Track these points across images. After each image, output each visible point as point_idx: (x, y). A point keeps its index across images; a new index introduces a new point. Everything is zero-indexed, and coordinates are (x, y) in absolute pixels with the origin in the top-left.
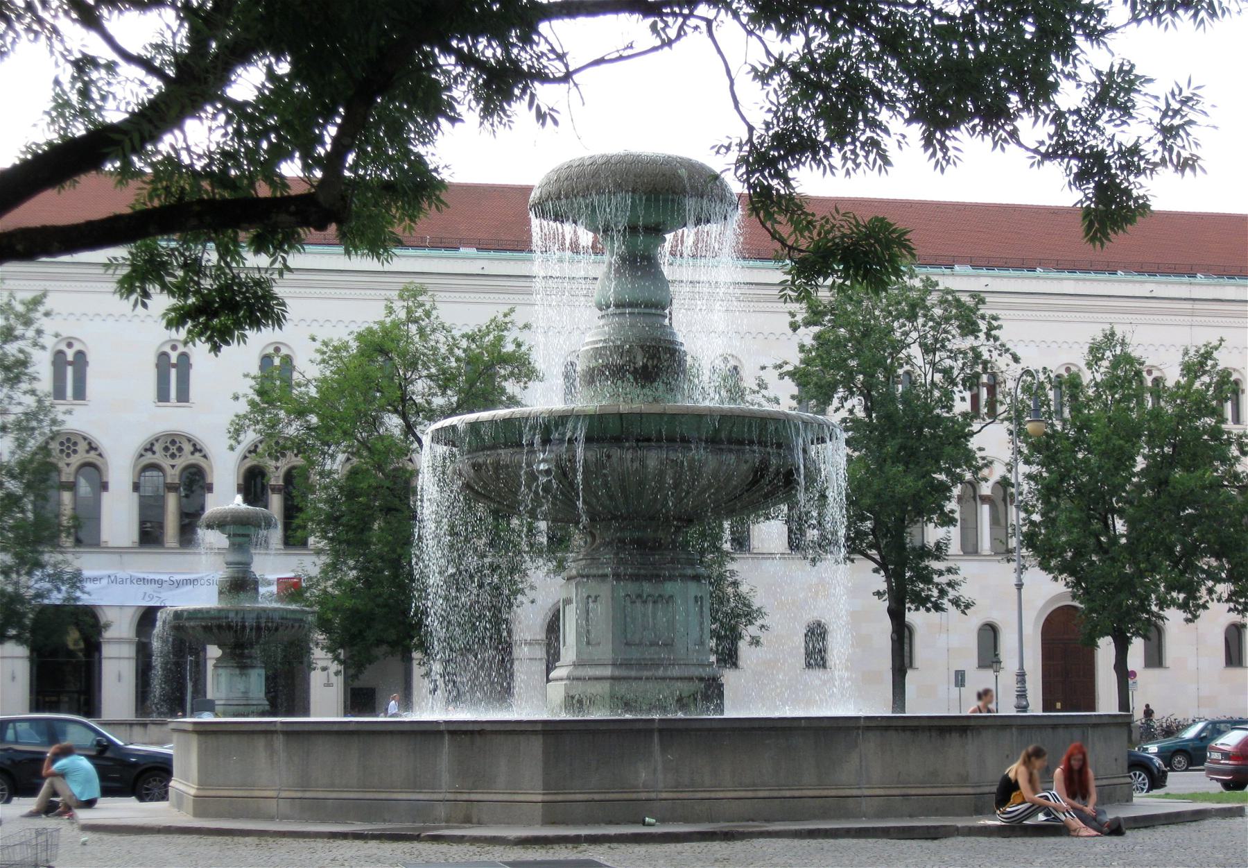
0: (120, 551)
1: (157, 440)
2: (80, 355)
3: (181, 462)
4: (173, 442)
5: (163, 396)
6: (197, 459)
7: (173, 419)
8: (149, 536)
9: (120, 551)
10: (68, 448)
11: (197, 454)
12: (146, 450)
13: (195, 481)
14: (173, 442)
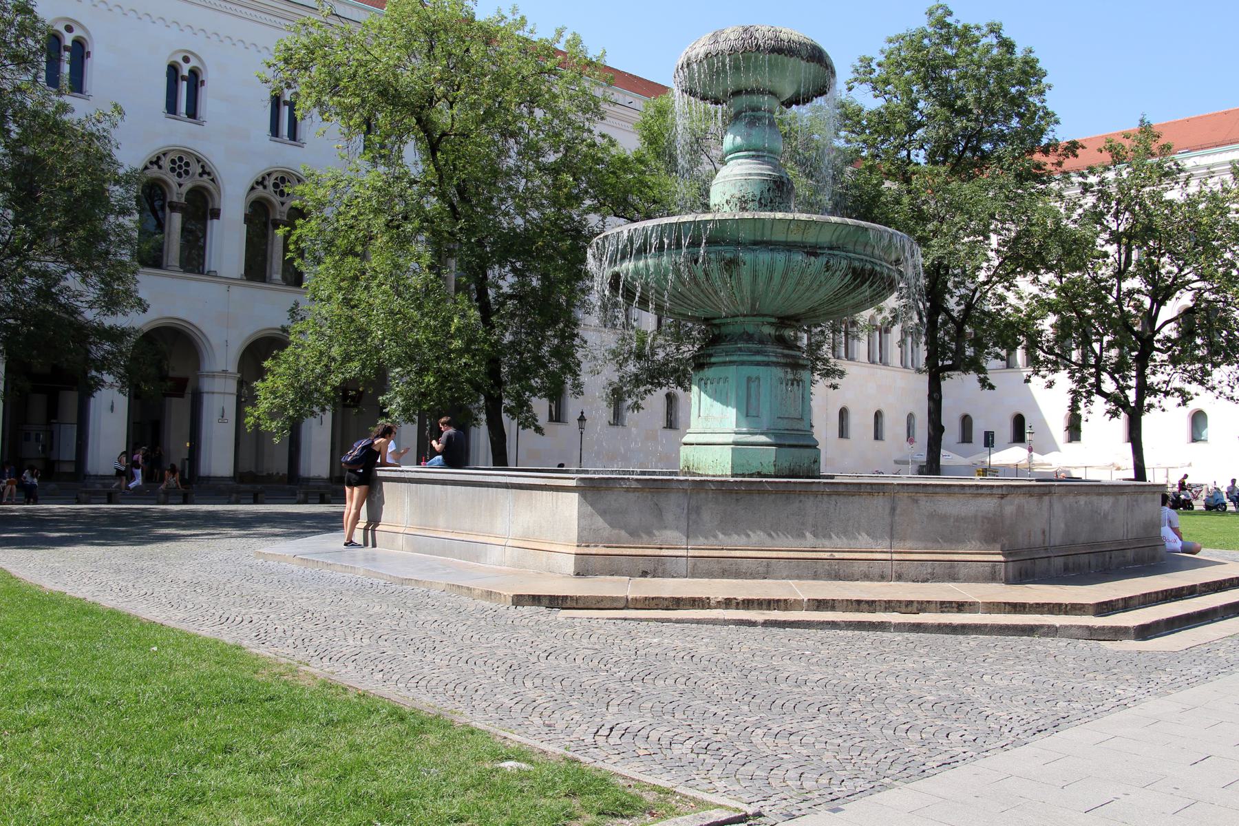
0: (229, 281)
1: (269, 175)
2: (194, 73)
3: (188, 184)
4: (181, 159)
5: (172, 108)
6: (211, 186)
7: (178, 134)
8: (256, 269)
9: (229, 281)
10: (180, 167)
11: (205, 177)
12: (151, 163)
13: (201, 207)
14: (181, 159)
